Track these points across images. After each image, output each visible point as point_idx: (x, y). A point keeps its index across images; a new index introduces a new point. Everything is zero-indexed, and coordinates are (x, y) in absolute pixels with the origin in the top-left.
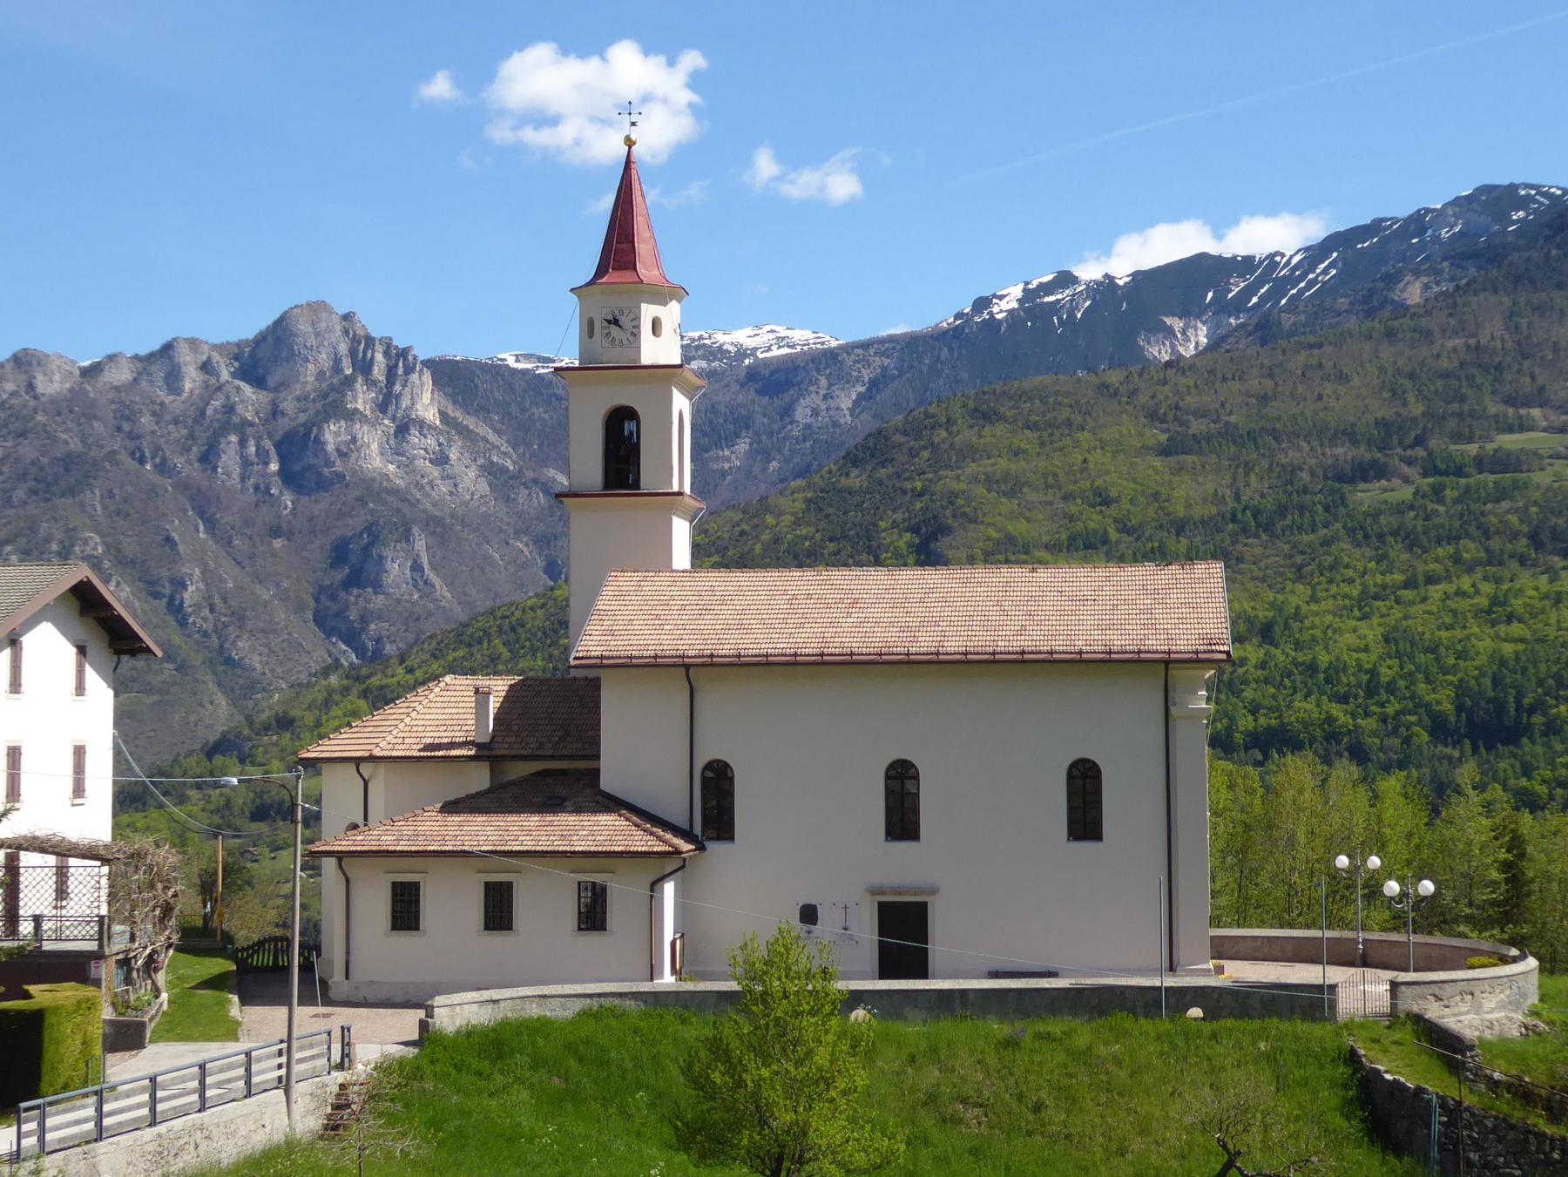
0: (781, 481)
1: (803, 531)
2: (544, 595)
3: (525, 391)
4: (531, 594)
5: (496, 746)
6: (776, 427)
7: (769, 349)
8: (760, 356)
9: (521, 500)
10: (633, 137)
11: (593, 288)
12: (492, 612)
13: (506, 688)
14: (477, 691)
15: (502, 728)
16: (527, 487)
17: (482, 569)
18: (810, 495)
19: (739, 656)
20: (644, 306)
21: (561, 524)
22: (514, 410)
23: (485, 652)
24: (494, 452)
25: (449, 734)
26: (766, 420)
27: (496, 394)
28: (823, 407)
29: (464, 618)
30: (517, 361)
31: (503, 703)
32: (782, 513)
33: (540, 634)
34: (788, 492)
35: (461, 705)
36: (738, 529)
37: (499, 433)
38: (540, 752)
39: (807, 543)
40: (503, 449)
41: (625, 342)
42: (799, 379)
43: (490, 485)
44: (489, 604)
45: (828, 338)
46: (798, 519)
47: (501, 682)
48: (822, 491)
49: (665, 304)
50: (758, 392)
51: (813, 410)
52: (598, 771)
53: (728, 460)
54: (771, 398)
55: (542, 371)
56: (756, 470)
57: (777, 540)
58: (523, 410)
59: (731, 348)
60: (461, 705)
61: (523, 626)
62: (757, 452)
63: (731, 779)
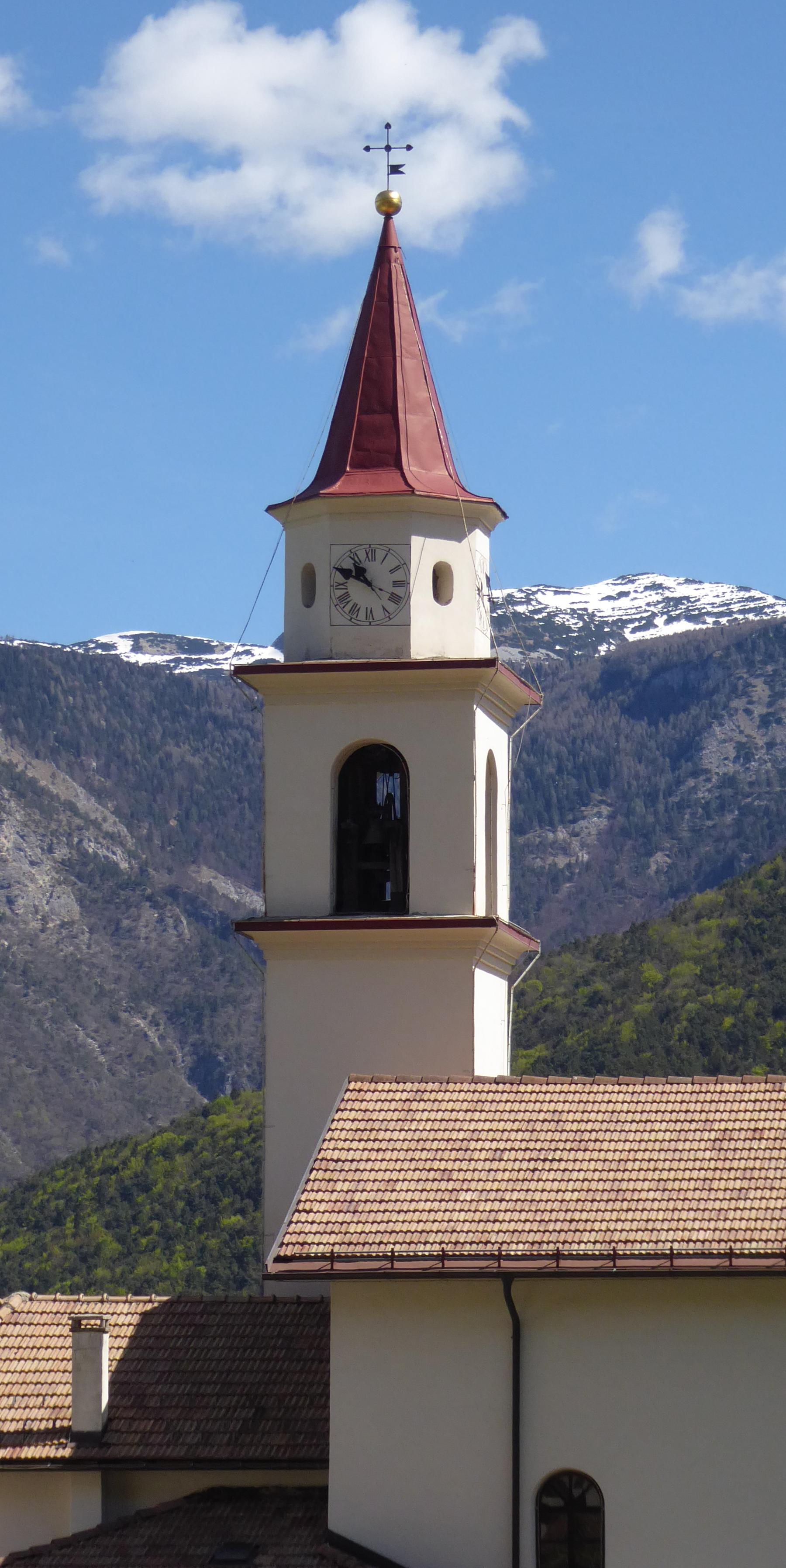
0: (674, 893)
1: (721, 995)
2: (190, 1125)
3: (152, 709)
4: (164, 1123)
5: (111, 1438)
6: (663, 781)
7: (649, 623)
8: (631, 637)
9: (143, 932)
10: (395, 196)
11: (315, 505)
12: (83, 1159)
13: (135, 1319)
14: (76, 1325)
15: (127, 1402)
16: (155, 906)
17: (64, 1073)
18: (733, 921)
19: (614, 1256)
20: (416, 541)
21: (224, 981)
22: (130, 746)
23: (70, 1241)
24: (90, 833)
25: (18, 1414)
26: (641, 769)
27: (95, 717)
28: (760, 742)
29: (25, 1170)
30: (136, 649)
31: (128, 1349)
32: (676, 958)
33: (181, 1204)
34: (688, 915)
35: (42, 1354)
36: (585, 990)
37: (99, 794)
38: (204, 1453)
39: (728, 1021)
40: (107, 827)
41: (379, 614)
42: (711, 684)
43: (81, 901)
44: (78, 1142)
45: (770, 600)
46: (710, 970)
47: (125, 1308)
48: (759, 912)
49: (459, 537)
50: (628, 711)
51: (740, 746)
52: (323, 1492)
53: (565, 850)
54: (653, 723)
55: (186, 669)
56: (623, 869)
57: (666, 1014)
58: (150, 748)
59: (574, 623)
60: (42, 1354)
61: (146, 1188)
62: (625, 833)
63: (599, 1511)
